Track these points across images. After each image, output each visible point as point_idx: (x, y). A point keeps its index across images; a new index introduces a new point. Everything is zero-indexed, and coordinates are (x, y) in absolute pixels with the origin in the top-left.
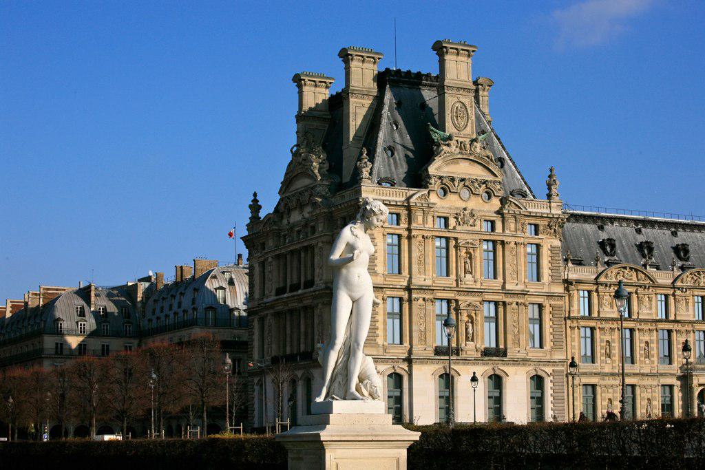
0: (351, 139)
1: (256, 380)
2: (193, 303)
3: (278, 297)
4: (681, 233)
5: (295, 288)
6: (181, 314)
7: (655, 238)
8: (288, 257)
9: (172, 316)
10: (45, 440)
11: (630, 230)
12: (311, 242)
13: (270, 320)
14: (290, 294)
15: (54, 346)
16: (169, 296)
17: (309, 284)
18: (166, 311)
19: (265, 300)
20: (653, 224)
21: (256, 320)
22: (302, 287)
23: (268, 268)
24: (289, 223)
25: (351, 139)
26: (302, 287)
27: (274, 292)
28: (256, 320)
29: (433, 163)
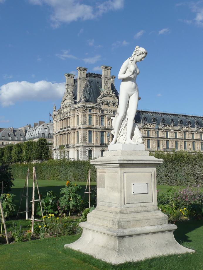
0: (190, 251)
1: (55, 152)
2: (39, 132)
3: (61, 130)
4: (154, 115)
5: (65, 128)
6: (35, 135)
7: (156, 117)
8: (63, 120)
9: (33, 135)
10: (142, 50)
11: (150, 114)
12: (69, 117)
13: (58, 136)
14: (64, 130)
15: (2, 143)
16: (32, 131)
17: (69, 127)
18: (32, 134)
19: (57, 131)
20: (156, 113)
21: (55, 136)
22: (67, 128)
23: (58, 123)
24: (25, 140)
25: (190, 251)
26: (67, 128)
27: (59, 129)
28: (55, 136)
29: (14, 82)
